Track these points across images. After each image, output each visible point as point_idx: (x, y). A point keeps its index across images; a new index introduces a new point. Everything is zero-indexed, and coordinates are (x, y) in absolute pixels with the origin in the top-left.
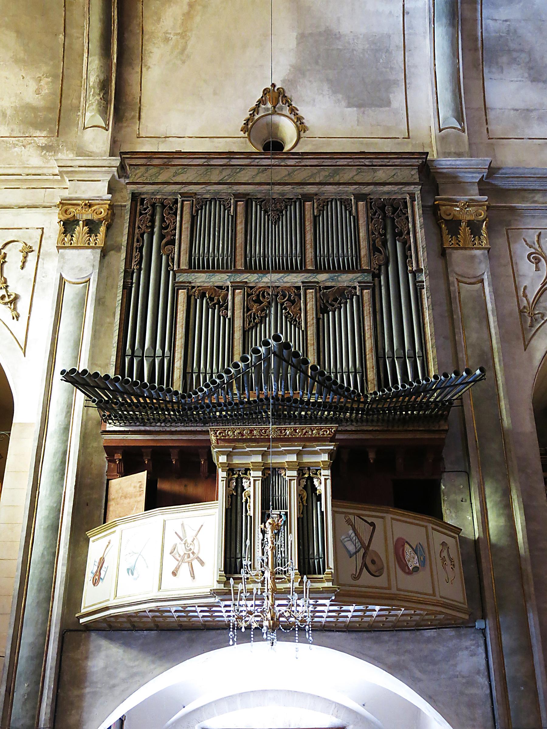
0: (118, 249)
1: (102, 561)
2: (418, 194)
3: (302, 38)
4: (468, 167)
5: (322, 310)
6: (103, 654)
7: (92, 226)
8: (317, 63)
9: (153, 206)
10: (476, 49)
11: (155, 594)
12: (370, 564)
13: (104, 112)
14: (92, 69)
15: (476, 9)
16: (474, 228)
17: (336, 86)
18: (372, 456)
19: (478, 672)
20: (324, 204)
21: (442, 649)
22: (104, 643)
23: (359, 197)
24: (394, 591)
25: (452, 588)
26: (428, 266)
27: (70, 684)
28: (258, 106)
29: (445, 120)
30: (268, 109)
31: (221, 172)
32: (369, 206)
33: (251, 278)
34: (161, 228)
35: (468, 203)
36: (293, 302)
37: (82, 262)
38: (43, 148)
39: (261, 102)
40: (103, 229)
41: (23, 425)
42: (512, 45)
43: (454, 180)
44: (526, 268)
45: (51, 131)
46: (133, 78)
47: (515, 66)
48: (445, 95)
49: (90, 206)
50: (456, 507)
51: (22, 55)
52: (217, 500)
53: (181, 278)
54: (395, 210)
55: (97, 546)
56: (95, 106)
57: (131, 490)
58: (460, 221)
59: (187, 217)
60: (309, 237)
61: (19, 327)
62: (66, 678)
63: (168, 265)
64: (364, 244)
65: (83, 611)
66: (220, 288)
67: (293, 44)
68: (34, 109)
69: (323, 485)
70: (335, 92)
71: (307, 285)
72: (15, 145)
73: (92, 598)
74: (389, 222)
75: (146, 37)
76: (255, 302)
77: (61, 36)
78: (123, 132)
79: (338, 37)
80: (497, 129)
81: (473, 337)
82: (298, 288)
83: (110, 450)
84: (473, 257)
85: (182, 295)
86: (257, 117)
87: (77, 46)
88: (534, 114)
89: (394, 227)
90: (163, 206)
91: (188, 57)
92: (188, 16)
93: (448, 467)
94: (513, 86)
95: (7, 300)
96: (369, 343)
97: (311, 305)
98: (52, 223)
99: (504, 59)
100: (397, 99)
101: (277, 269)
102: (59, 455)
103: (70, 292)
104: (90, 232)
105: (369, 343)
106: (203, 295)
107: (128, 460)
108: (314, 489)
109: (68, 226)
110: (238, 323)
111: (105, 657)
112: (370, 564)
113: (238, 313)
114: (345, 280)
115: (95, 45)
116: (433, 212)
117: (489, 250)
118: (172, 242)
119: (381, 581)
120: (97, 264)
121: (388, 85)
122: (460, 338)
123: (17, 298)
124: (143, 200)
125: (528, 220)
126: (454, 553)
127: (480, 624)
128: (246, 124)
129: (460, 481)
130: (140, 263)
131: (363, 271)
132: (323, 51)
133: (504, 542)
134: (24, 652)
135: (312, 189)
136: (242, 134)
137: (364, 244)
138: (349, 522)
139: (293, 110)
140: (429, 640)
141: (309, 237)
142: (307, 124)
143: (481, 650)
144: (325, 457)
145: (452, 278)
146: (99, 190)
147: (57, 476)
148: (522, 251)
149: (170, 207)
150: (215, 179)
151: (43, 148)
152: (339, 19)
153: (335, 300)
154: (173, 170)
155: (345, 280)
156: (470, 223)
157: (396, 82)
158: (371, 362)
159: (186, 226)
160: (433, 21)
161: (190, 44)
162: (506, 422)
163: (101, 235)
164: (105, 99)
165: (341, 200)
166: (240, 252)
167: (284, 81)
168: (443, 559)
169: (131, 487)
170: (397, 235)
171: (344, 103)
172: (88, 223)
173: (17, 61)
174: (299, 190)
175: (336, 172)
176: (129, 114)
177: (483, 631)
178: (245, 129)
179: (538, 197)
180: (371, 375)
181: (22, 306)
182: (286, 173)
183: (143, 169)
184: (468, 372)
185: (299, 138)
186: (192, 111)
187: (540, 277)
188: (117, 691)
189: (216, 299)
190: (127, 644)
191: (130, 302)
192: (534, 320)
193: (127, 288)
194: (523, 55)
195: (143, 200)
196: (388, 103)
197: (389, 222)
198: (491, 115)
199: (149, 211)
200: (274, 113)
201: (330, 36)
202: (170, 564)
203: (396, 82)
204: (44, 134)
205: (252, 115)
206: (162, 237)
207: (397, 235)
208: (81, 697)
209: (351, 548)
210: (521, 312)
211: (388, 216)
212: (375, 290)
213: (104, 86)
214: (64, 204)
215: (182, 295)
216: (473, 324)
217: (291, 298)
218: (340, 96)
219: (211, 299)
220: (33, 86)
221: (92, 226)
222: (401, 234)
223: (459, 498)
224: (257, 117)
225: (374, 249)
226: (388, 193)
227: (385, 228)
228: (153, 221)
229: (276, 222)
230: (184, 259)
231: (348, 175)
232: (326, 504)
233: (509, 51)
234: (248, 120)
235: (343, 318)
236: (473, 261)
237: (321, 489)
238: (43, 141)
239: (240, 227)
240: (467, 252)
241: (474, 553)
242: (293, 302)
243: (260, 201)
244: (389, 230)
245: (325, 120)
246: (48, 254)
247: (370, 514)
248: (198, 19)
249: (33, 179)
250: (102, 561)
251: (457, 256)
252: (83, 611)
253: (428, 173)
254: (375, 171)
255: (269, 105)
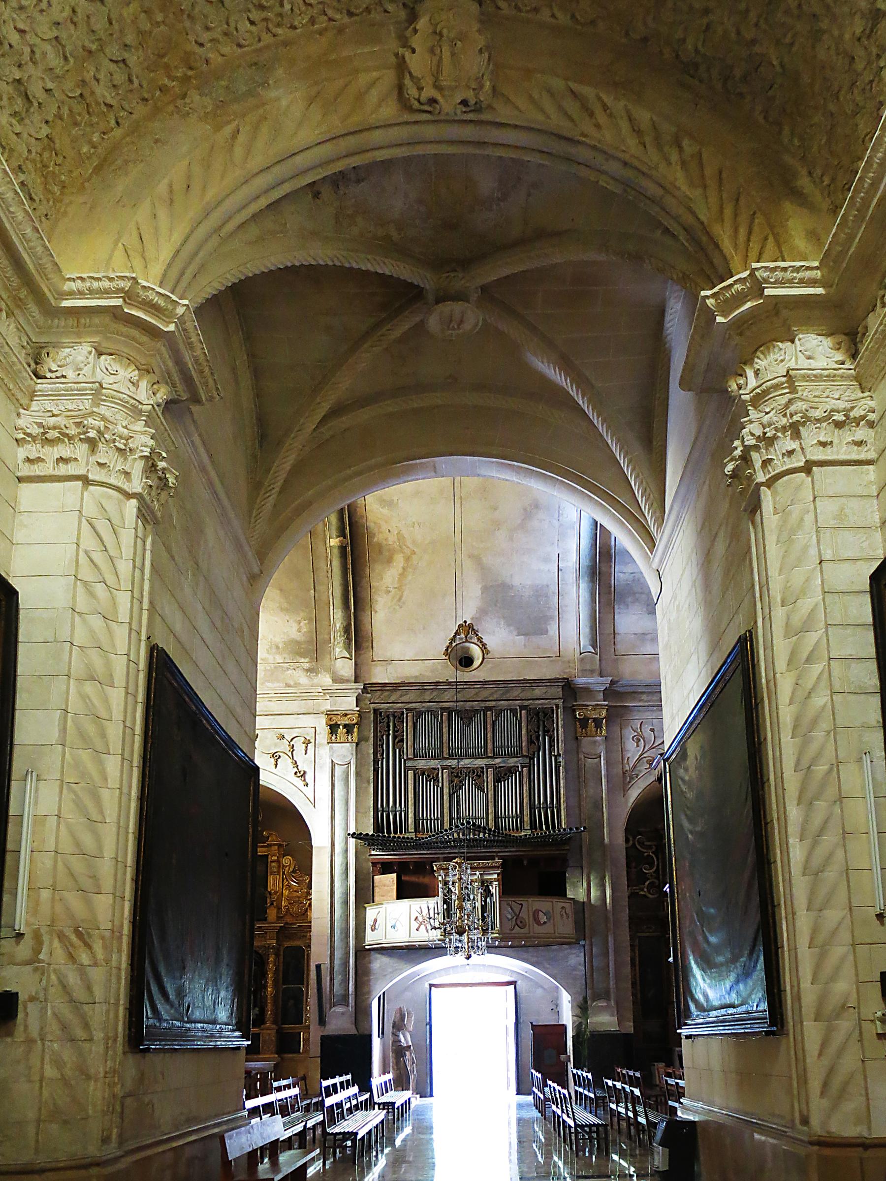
0: (367, 740)
1: (375, 921)
2: (561, 705)
3: (485, 589)
4: (597, 683)
5: (498, 780)
6: (378, 961)
7: (349, 728)
8: (496, 605)
9: (388, 717)
10: (610, 593)
11: (407, 939)
12: (520, 923)
13: (348, 648)
14: (337, 618)
15: (611, 566)
16: (598, 723)
17: (510, 622)
18: (525, 863)
19: (580, 964)
20: (499, 712)
21: (561, 954)
22: (379, 956)
23: (522, 708)
24: (532, 934)
25: (566, 927)
26: (565, 752)
27: (363, 975)
28: (455, 636)
29: (584, 646)
30: (461, 639)
31: (431, 693)
32: (528, 714)
33: (453, 763)
34: (394, 731)
35: (595, 707)
36: (479, 776)
37: (345, 751)
38: (307, 670)
39: (457, 633)
40: (356, 730)
41: (320, 848)
42: (635, 589)
43: (587, 691)
44: (631, 745)
45: (312, 658)
46: (366, 619)
47: (637, 604)
48: (585, 630)
49: (346, 715)
50: (575, 886)
51: (285, 605)
52: (431, 1096)
53: (409, 764)
54: (545, 715)
55: (371, 913)
56: (341, 645)
57: (387, 882)
58: (589, 719)
59: (410, 724)
60: (489, 735)
61: (309, 791)
62: (360, 972)
63: (400, 755)
64: (524, 738)
65: (367, 943)
66: (434, 769)
67: (479, 593)
68: (298, 643)
69: (494, 889)
70: (509, 625)
71: (488, 766)
72: (288, 669)
73: (371, 938)
74: (541, 723)
75: (373, 590)
76: (456, 777)
77: (312, 591)
78: (362, 657)
79: (511, 587)
80: (621, 648)
81: (591, 791)
82: (483, 768)
83: (374, 864)
84: (595, 742)
85: (411, 774)
86: (454, 644)
87: (324, 598)
88: (649, 637)
89: (544, 726)
90: (395, 717)
91: (404, 603)
92: (403, 575)
93: (571, 863)
94: (635, 617)
95: (298, 774)
96: (526, 800)
97: (491, 778)
98: (321, 723)
99: (630, 599)
100: (553, 629)
101: (468, 757)
102: (344, 865)
103: (338, 770)
104: (348, 733)
105: (526, 800)
106: (423, 774)
107: (386, 868)
108: (490, 891)
109: (333, 728)
110: (446, 791)
111: (379, 963)
112: (520, 923)
113: (446, 784)
114: (512, 762)
115: (338, 601)
116: (570, 711)
117: (606, 737)
118: (402, 741)
119: (525, 930)
120: (354, 753)
121: (546, 619)
122: (583, 792)
123: (305, 772)
124: (381, 713)
125: (635, 713)
126: (569, 911)
127: (582, 943)
128: (447, 650)
129: (577, 872)
130: (382, 755)
131: (523, 756)
132: (500, 597)
133: (598, 903)
134: (337, 962)
135: (493, 704)
136: (444, 657)
137: (524, 738)
138: (508, 904)
139: (480, 639)
140: (554, 950)
141: (489, 735)
142: (489, 649)
143: (582, 954)
144: (495, 876)
145: (581, 756)
146: (349, 703)
147: (344, 876)
148: (629, 734)
149: (399, 717)
150: (427, 699)
151: (307, 670)
152: (511, 575)
153: (506, 774)
154: (399, 693)
155: (512, 762)
156: (595, 720)
157: (552, 618)
158: (526, 811)
159: (410, 730)
160: (578, 579)
161: (405, 594)
162: (606, 840)
163: (355, 734)
164: (349, 639)
165: (511, 710)
166: (445, 745)
167: (472, 619)
168: (562, 915)
169: (387, 882)
170: (546, 732)
171: (515, 633)
172: (345, 726)
173: (282, 609)
174: (483, 704)
175: (508, 692)
176: (365, 645)
177: (584, 946)
178: (446, 653)
179: (644, 697)
180: (526, 818)
181: (309, 778)
182: (474, 693)
183: (379, 693)
184: (577, 829)
185: (483, 658)
186: (408, 648)
187: (639, 751)
188: (388, 977)
189: (432, 775)
190: (390, 956)
191: (375, 773)
192: (632, 778)
193: (376, 771)
194: (644, 596)
195: (381, 713)
196: (546, 632)
197: (541, 723)
198: (618, 638)
199: (386, 720)
200: (467, 641)
201: (505, 587)
202: (415, 925)
203: (552, 618)
204: (307, 660)
205: (451, 643)
206: (395, 738)
207: (546, 732)
208: (369, 981)
209: (509, 917)
210: (624, 773)
211: (541, 719)
212: (530, 767)
213: (347, 630)
214: (329, 714)
215: (411, 774)
216: (591, 784)
217: (478, 774)
218: (512, 628)
219: (429, 776)
220: (295, 626)
221: (349, 728)
222: (548, 731)
223: (576, 880)
224: (454, 644)
225: (530, 742)
226: (542, 704)
227: (538, 728)
228: (388, 726)
229: (469, 726)
230: (410, 751)
231: (515, 693)
232: (496, 898)
233: (634, 593)
234: (448, 647)
235: (509, 788)
236: (596, 744)
237: (493, 891)
238: (307, 666)
239: (445, 730)
240: (591, 739)
241: (581, 908)
242: (479, 776)
243: (458, 712)
244: (541, 728)
245: (503, 648)
246: (320, 745)
247: (520, 900)
248: (410, 578)
249: (306, 695)
250: (375, 921)
251: (585, 741)
252: (367, 943)
253: (569, 688)
254: (533, 690)
255: (463, 636)
